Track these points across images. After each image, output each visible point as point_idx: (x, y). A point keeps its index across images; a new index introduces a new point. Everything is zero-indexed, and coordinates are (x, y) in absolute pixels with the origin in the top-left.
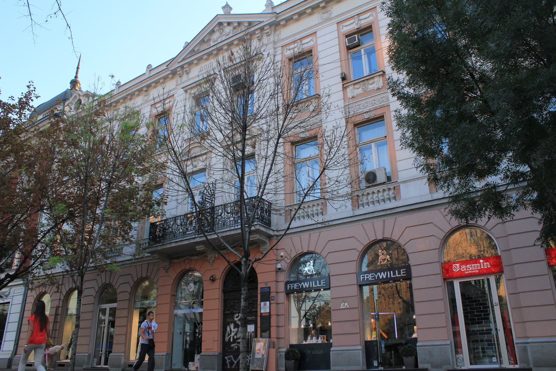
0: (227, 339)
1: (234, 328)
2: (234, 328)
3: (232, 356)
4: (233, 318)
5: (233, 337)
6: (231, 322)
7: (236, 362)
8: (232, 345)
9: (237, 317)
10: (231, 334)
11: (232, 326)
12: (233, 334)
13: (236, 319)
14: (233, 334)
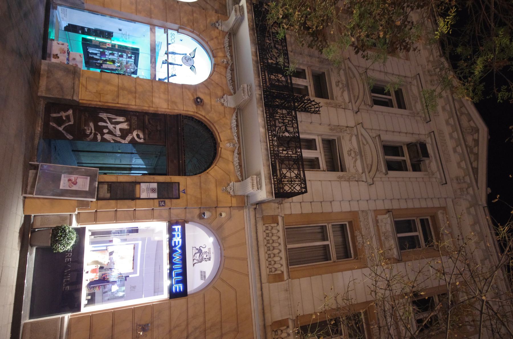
0: (104, 116)
1: (121, 130)
2: (121, 130)
3: (72, 123)
4: (138, 128)
5: (106, 127)
6: (130, 125)
7: (61, 129)
8: (91, 124)
9: (138, 136)
10: (112, 123)
11: (125, 126)
12: (111, 126)
13: (135, 133)
14: (111, 126)
